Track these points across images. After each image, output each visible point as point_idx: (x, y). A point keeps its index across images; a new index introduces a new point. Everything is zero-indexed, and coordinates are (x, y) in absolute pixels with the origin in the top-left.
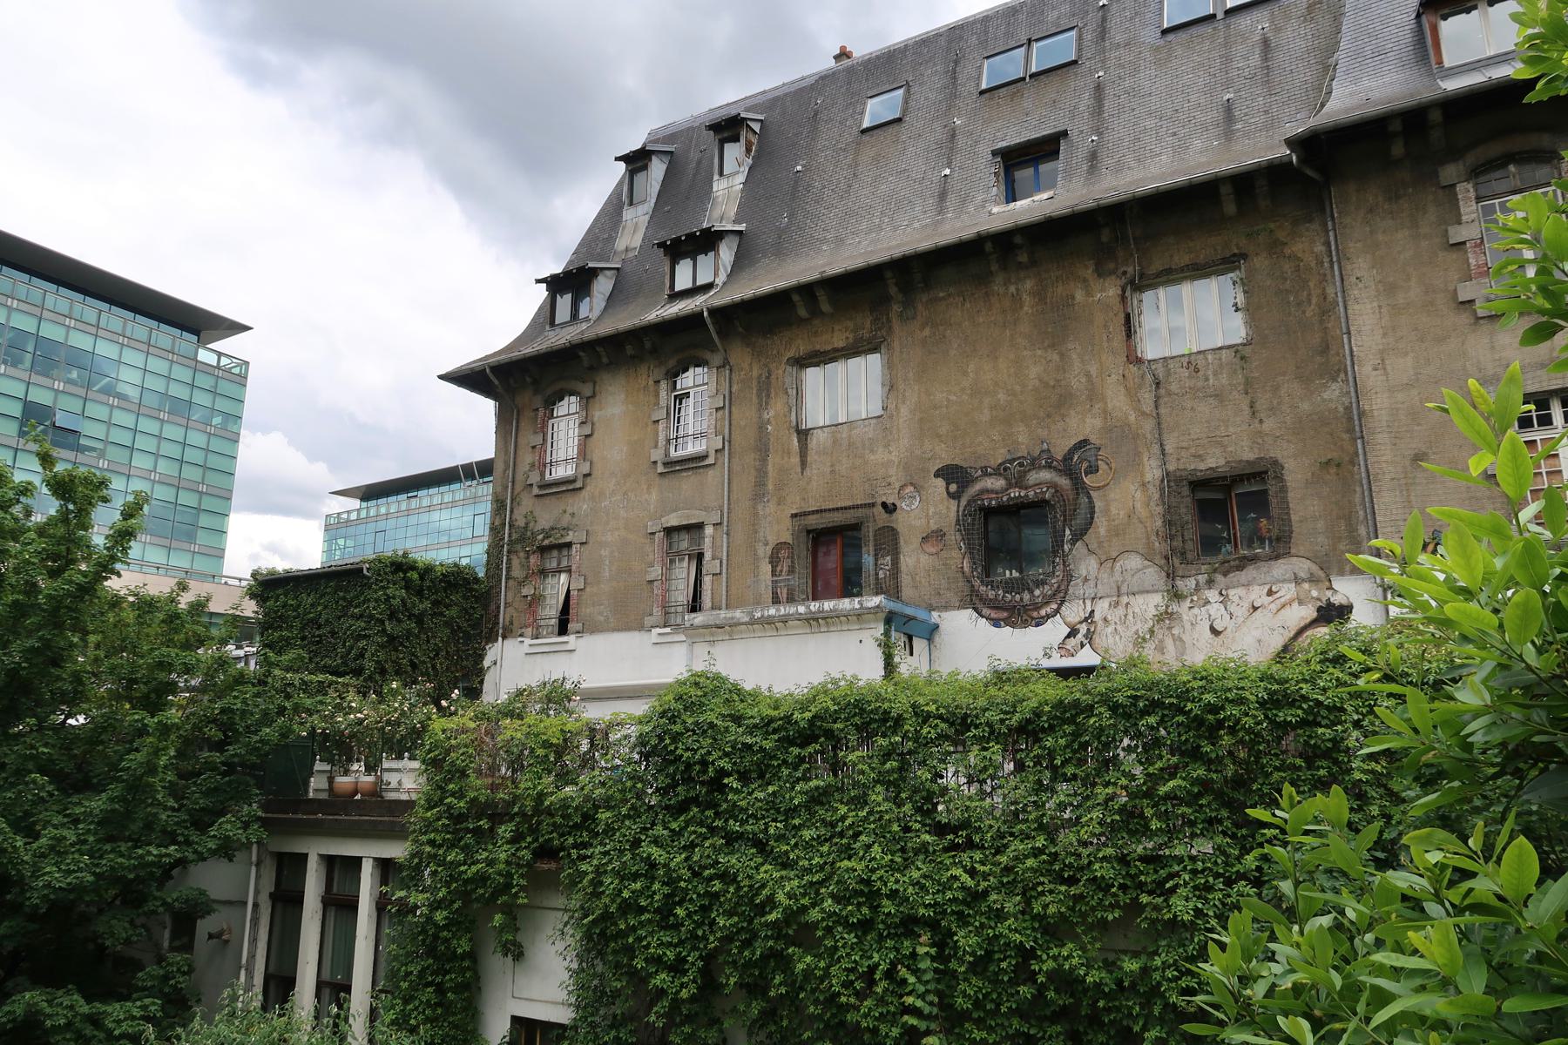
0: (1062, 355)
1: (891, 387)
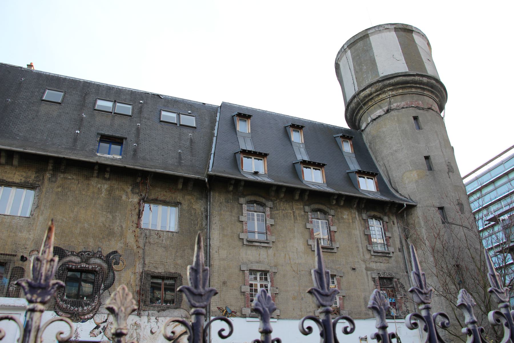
0: (113, 217)
1: (37, 206)
